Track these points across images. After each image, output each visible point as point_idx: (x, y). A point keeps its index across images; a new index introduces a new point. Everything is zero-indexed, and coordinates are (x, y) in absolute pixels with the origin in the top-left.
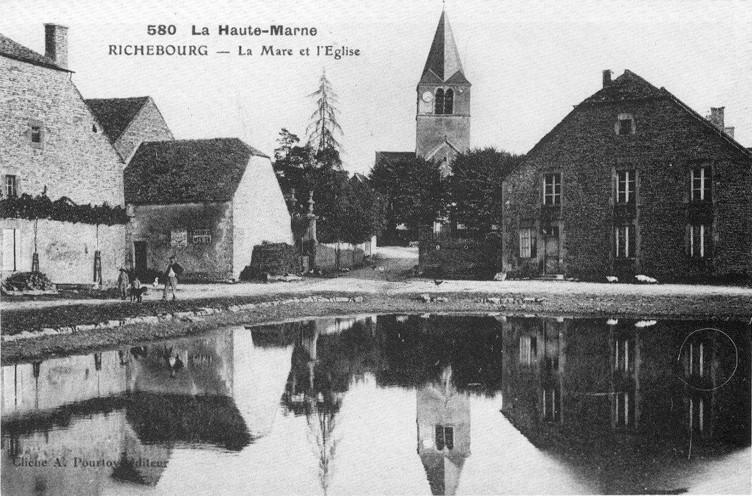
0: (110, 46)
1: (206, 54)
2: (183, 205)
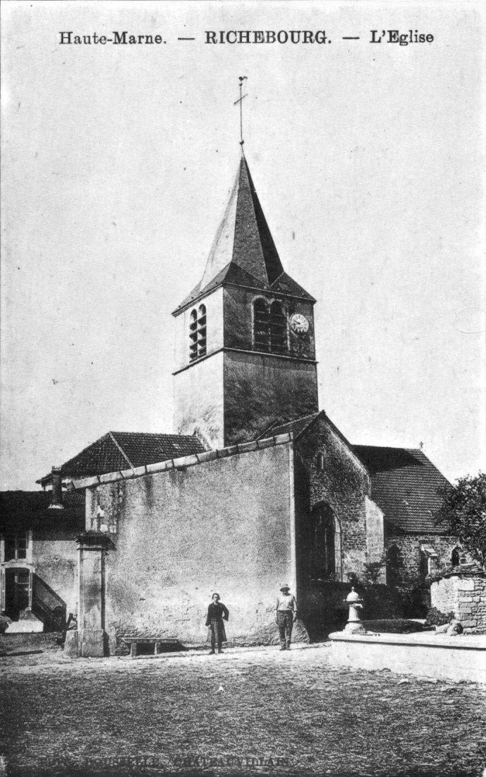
0: (208, 33)
2: (253, 331)
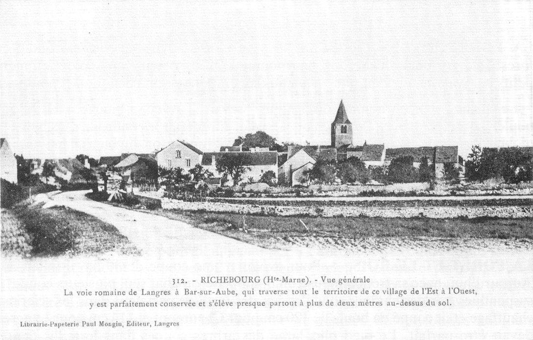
1: (307, 246)
